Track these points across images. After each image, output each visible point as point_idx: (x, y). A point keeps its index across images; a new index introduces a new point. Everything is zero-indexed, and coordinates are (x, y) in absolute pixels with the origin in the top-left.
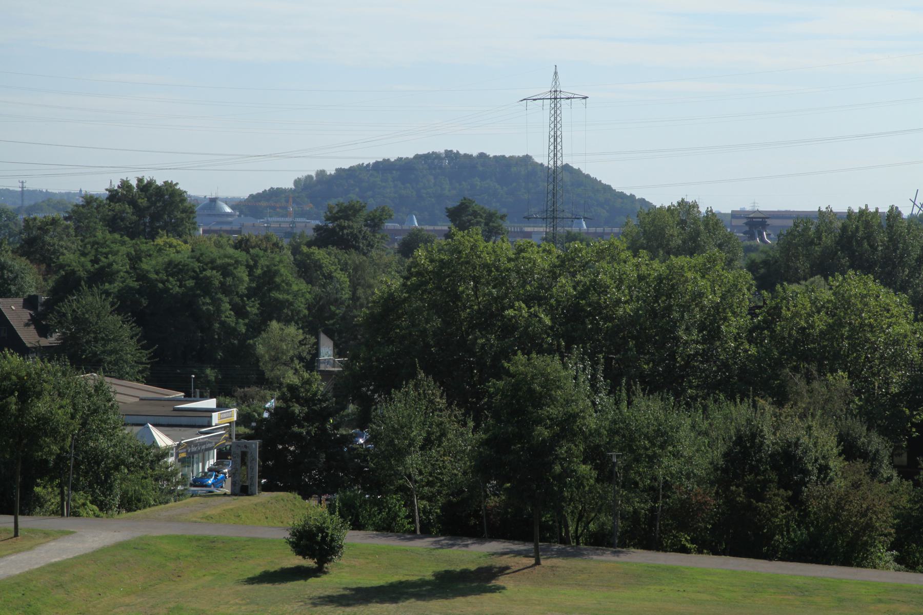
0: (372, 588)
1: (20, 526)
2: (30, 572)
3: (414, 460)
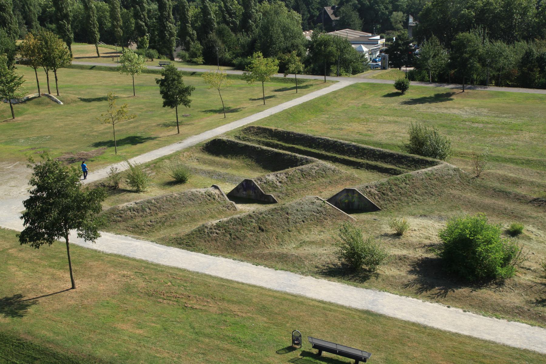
3: (430, 61)
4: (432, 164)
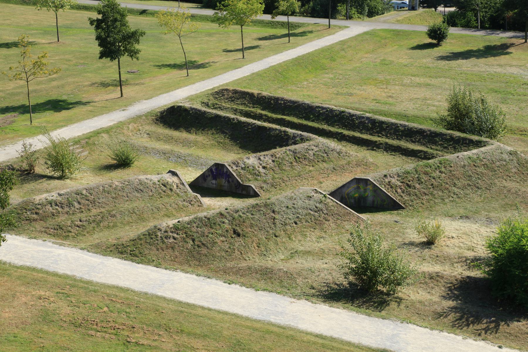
0: (458, 53)
1: (331, 23)
2: (333, 44)
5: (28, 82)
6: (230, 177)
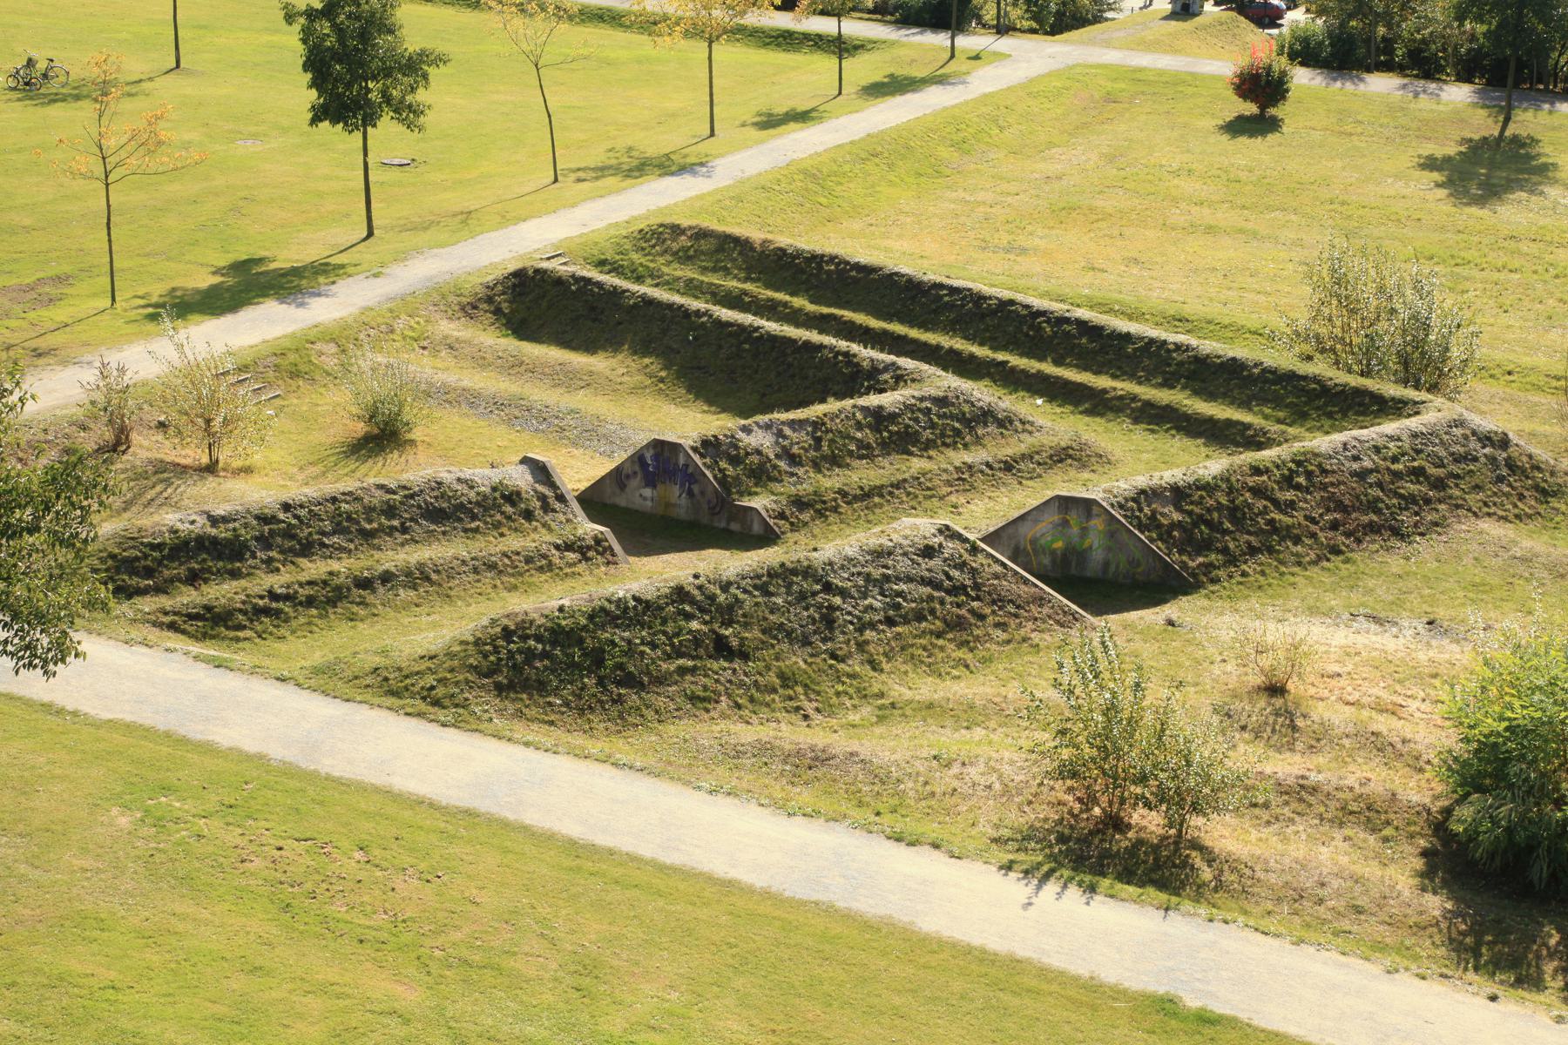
4: (1397, 408)
5: (107, 185)
6: (696, 481)
